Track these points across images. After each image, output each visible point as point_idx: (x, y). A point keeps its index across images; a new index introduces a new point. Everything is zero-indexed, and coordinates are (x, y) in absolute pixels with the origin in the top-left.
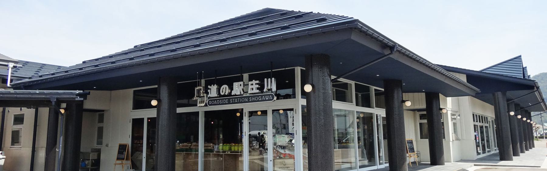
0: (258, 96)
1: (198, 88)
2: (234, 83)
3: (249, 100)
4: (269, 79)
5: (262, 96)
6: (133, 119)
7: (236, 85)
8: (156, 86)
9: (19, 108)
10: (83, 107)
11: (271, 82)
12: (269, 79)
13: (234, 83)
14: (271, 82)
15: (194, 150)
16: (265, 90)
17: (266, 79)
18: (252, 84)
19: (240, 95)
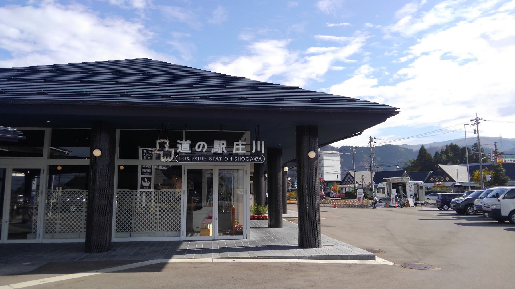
0: (245, 157)
1: (162, 141)
2: (215, 141)
3: (233, 159)
4: (259, 142)
5: (250, 157)
6: (188, 170)
7: (216, 143)
8: (118, 131)
9: (433, 9)
10: (250, 132)
11: (261, 145)
12: (259, 142)
13: (215, 141)
14: (261, 145)
15: (54, 190)
16: (253, 152)
17: (254, 142)
18: (238, 145)
19: (222, 154)
